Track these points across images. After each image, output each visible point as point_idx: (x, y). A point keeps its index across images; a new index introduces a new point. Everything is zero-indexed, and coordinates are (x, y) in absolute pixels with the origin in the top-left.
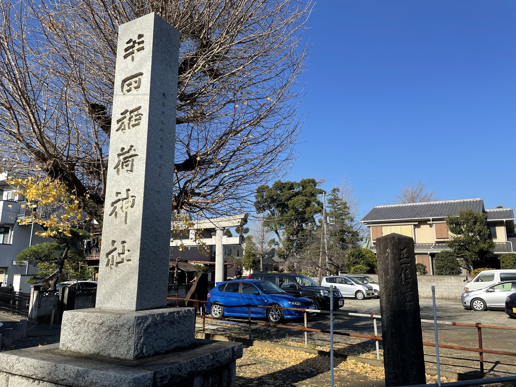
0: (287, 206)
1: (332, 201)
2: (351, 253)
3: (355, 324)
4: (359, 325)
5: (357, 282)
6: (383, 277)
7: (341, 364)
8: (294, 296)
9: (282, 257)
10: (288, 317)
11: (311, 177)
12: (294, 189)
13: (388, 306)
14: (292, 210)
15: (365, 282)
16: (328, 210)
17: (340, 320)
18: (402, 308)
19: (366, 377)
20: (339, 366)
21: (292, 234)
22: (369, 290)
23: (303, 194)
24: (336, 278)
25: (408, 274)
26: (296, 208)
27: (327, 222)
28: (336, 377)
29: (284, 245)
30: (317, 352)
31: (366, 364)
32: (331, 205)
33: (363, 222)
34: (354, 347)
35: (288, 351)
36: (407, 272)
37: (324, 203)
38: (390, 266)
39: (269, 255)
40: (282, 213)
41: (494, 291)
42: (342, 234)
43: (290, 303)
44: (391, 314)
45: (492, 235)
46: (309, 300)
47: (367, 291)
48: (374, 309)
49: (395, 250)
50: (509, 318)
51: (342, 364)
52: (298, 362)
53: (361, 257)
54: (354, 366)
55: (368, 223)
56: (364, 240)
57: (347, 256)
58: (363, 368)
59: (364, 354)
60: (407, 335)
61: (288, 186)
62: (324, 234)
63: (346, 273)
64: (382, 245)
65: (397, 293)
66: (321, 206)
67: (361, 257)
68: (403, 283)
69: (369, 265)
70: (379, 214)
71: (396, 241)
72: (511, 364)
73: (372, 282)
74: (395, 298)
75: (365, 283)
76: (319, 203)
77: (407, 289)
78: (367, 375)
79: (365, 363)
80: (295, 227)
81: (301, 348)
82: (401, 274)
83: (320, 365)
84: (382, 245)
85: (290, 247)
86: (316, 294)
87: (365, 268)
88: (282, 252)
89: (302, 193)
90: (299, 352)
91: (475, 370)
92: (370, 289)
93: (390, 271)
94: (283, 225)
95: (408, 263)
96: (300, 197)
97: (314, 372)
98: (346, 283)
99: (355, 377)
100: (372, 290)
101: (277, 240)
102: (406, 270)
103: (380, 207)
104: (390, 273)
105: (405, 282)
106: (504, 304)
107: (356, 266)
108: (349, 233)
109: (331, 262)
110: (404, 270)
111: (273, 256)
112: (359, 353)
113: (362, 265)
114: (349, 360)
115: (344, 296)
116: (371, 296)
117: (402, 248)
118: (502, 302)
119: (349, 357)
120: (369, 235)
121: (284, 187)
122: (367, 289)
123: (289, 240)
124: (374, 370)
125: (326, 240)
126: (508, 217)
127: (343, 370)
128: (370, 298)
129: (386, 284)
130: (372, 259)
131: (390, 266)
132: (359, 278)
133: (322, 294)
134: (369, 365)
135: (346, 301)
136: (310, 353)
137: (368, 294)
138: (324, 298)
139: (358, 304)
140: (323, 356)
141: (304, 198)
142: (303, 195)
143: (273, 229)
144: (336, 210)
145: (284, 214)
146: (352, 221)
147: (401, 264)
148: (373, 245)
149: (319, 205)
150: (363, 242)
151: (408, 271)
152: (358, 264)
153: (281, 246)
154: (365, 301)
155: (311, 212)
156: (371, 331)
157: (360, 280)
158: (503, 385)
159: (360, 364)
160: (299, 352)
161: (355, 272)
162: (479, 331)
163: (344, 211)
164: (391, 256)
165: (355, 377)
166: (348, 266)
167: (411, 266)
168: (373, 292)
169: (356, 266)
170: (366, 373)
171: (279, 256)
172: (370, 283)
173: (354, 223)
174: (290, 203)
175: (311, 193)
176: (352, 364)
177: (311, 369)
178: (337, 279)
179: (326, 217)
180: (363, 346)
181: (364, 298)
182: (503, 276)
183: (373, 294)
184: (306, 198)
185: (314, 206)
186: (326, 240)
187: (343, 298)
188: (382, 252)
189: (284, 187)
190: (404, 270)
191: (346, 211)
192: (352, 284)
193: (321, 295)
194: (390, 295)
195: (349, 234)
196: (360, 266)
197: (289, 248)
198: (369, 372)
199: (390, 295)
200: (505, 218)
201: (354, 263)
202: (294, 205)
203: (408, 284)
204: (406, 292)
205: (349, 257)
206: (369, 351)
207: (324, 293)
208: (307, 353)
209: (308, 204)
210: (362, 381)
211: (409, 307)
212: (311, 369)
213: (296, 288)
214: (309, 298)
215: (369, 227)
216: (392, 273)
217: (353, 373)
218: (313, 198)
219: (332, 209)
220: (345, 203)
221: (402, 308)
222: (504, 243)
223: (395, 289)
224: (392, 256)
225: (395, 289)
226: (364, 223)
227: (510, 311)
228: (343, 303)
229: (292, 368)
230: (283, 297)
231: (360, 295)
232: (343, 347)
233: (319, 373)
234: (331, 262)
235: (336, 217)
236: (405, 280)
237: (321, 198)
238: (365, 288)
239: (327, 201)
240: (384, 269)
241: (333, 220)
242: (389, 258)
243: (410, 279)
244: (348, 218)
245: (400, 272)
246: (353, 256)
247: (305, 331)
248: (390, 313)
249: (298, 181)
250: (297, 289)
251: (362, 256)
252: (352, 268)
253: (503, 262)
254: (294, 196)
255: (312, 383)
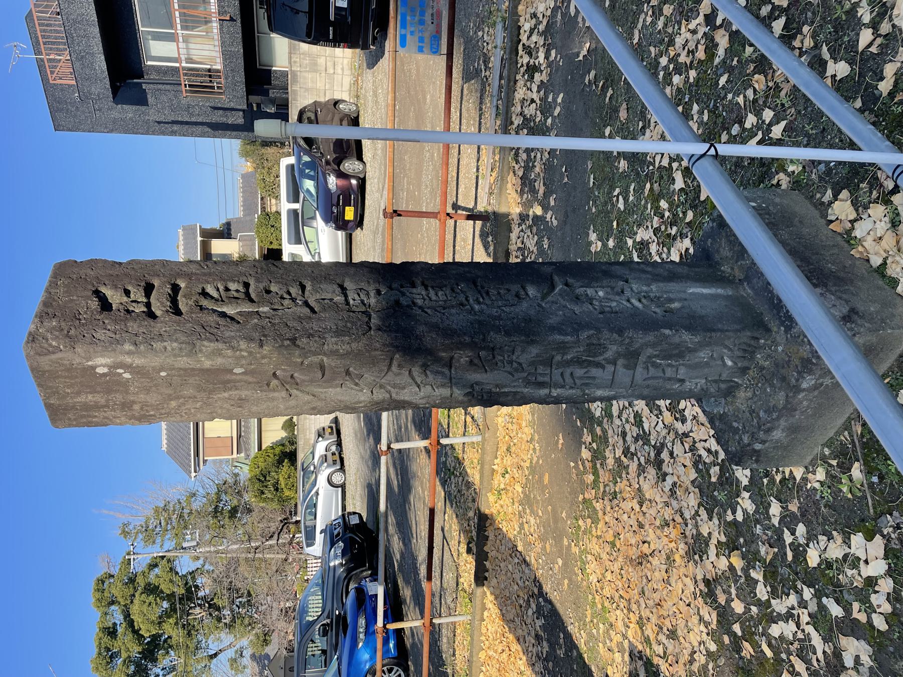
0: (155, 638)
1: (150, 536)
2: (256, 496)
3: (396, 489)
4: (398, 481)
5: (312, 484)
6: (244, 393)
7: (504, 530)
8: (345, 635)
9: (267, 638)
10: (391, 645)
11: (93, 585)
12: (115, 624)
13: (369, 377)
14: (166, 626)
15: (312, 468)
16: (169, 544)
17: (390, 521)
18: (375, 321)
19: (533, 469)
20: (512, 537)
21: (219, 620)
22: (326, 461)
23: (129, 602)
24: (306, 527)
25: (227, 289)
26: (160, 617)
27: (194, 547)
28: (548, 546)
29: (242, 637)
30: (479, 591)
31: (495, 467)
32: (159, 540)
33: (193, 474)
34: (450, 494)
35: (483, 669)
36: (215, 294)
37: (152, 555)
38: (183, 362)
39: (264, 667)
40: (171, 647)
41: (319, 253)
42: (222, 514)
43: (361, 645)
44: (400, 366)
45: (226, 260)
46: (352, 593)
47: (328, 466)
48: (362, 451)
49: (100, 334)
50: (362, 229)
51: (504, 527)
52: (516, 647)
53: (265, 477)
54: (504, 497)
55: (197, 464)
56: (236, 471)
57: (262, 505)
58: (507, 476)
59: (469, 471)
60: (477, 307)
61: (106, 640)
62: (217, 552)
63: (296, 505)
64: (81, 399)
65: (310, 336)
66: (158, 560)
67: (265, 477)
68: (265, 309)
69: (280, 462)
70: (179, 444)
71: (51, 330)
72: (455, 183)
73: (311, 455)
74: (332, 342)
75: (315, 468)
76: (153, 566)
77: (293, 300)
78: (527, 464)
79: (493, 470)
80: (204, 614)
81: (472, 630)
82: (223, 315)
83: (516, 587)
84: (81, 399)
85: (246, 621)
86: (339, 578)
87: (285, 469)
88: (258, 638)
89: (125, 606)
90: (483, 638)
91: (477, 240)
92: (325, 458)
93: (207, 364)
94: (199, 642)
95: (176, 288)
96: (135, 609)
97: (538, 606)
98: (315, 506)
99: (536, 494)
100: (326, 456)
101: (230, 653)
102: (205, 294)
103: (165, 442)
104: (219, 361)
105: (260, 303)
106: (339, 233)
107: (283, 486)
108: (219, 500)
109: (276, 536)
110: (205, 303)
111: (267, 656)
112: (469, 485)
113: (280, 475)
114: (489, 507)
115: (340, 513)
116: (337, 457)
117: (94, 304)
118: (336, 237)
119: (482, 510)
120: (227, 461)
121: (108, 649)
122: (325, 464)
123: (230, 626)
124: (508, 450)
125: (232, 547)
126: (195, 234)
127: (522, 524)
128: (342, 460)
129: (275, 382)
130: (268, 456)
131: (183, 362)
132: (306, 480)
133: (337, 562)
134: (496, 461)
135: (350, 509)
136: (484, 608)
137: (334, 462)
138: (347, 557)
139: (353, 482)
140: (487, 574)
141: (136, 601)
142: (132, 602)
143: (206, 666)
144: (169, 527)
145: (173, 642)
146: (194, 495)
147: (178, 312)
148: (243, 455)
149: (156, 565)
150: (240, 473)
151: (210, 290)
152: (277, 483)
153: (245, 642)
154: (347, 468)
155: (171, 581)
156: (408, 456)
157: (309, 478)
158: (511, 173)
159: (499, 481)
160: (483, 638)
161: (293, 487)
162: (400, 215)
163: (174, 511)
164: (129, 353)
165: (536, 494)
166: (282, 501)
167: (189, 276)
168: (329, 454)
169: (283, 486)
170: (519, 467)
171: (267, 645)
172: (313, 459)
173: (201, 490)
174: (147, 631)
175: (126, 584)
176: (501, 502)
177: (530, 612)
178: (309, 523)
179: (183, 548)
180: (445, 474)
181: (342, 468)
182: (293, 240)
183: (333, 454)
184: (137, 595)
185: (157, 576)
186: (232, 547)
187: (343, 515)
188: (119, 398)
189: (108, 649)
190: (205, 303)
191: (174, 507)
192: (317, 493)
193: (341, 564)
194: (322, 368)
195: (221, 500)
196: (281, 479)
197: (250, 624)
198: (516, 460)
199: (322, 368)
200: (195, 238)
201: (277, 490)
202: (153, 622)
203: (268, 292)
204: (306, 304)
205: (265, 500)
206: (459, 462)
207: (336, 557)
208: (485, 617)
209: (152, 590)
210: (547, 476)
211: (368, 294)
212: (530, 612)
213: (328, 624)
214: (347, 593)
215: (205, 461)
216: (218, 353)
217: (527, 501)
218: (140, 580)
219: (167, 537)
220: (156, 510)
221: (375, 321)
222: (241, 244)
223: (293, 340)
224: (128, 347)
225: (293, 340)
226: (195, 472)
227: (351, 224)
228: (354, 513)
229: (537, 669)
230: (350, 664)
231: (338, 478)
232: (455, 519)
233: (541, 593)
234: (276, 536)
235: (186, 528)
236: (252, 301)
237: (140, 563)
238: (323, 468)
239: (150, 548)
240: (199, 389)
241: (191, 534)
242: (138, 361)
243: (247, 285)
244: (189, 503)
245: (212, 319)
246: (263, 493)
247: (431, 623)
248: (394, 368)
249: (97, 614)
250: (328, 621)
251: (262, 474)
252: (287, 493)
253: (271, 243)
254: (131, 623)
255: (582, 619)
